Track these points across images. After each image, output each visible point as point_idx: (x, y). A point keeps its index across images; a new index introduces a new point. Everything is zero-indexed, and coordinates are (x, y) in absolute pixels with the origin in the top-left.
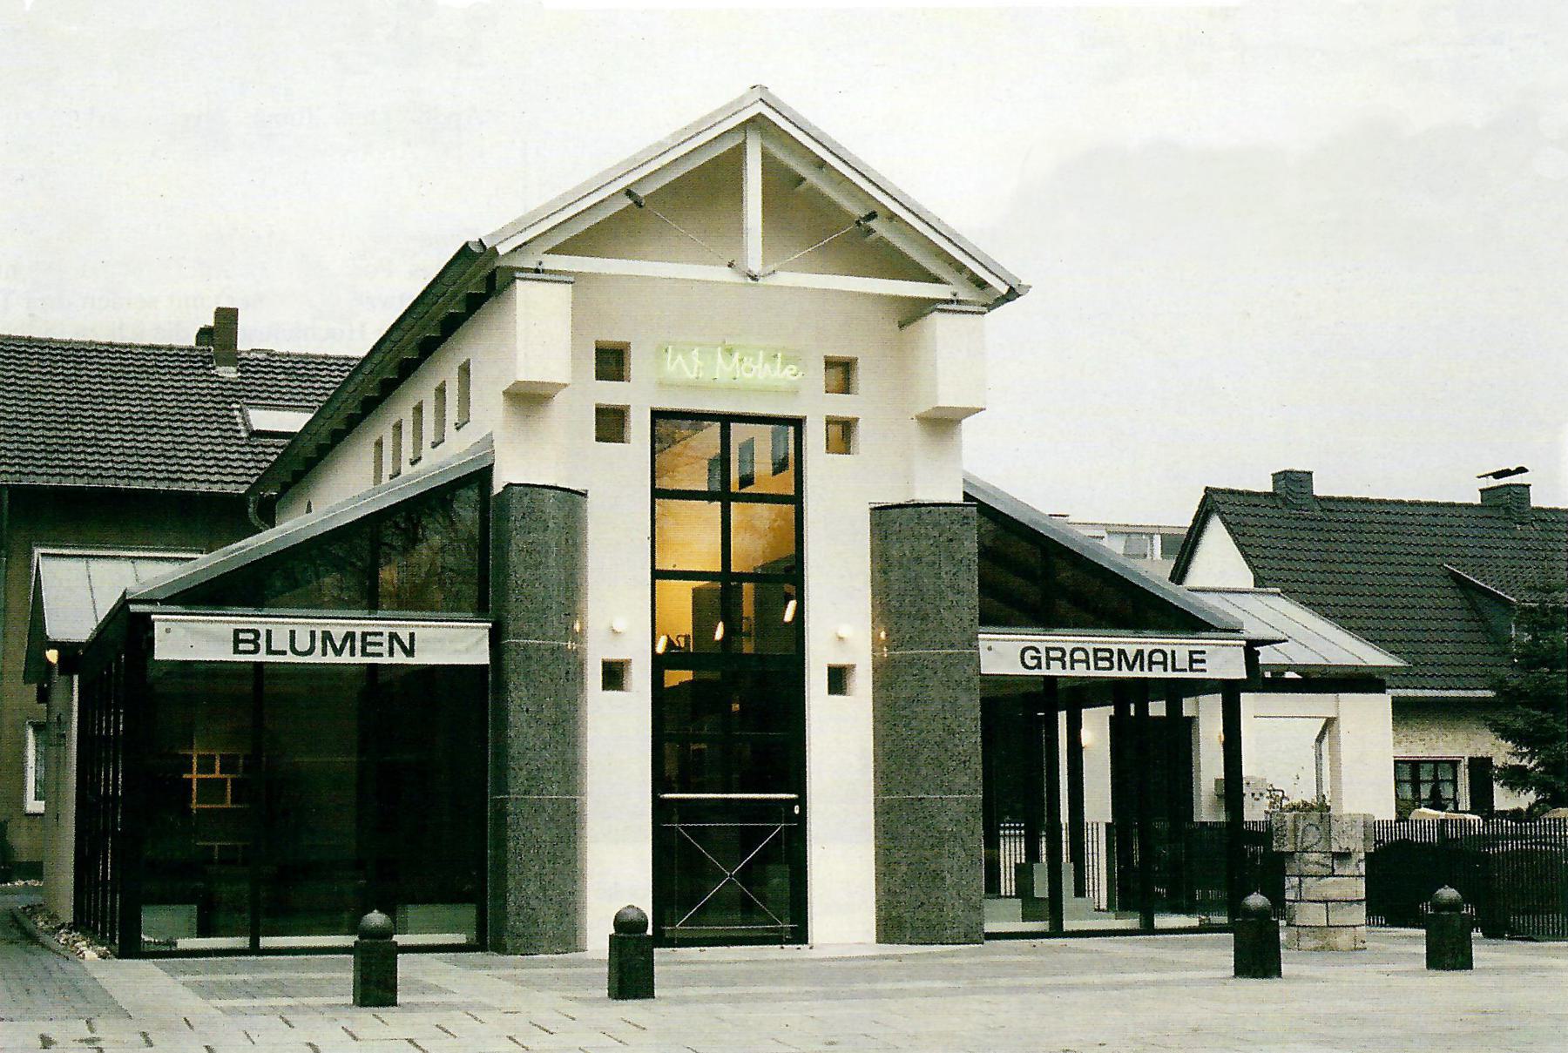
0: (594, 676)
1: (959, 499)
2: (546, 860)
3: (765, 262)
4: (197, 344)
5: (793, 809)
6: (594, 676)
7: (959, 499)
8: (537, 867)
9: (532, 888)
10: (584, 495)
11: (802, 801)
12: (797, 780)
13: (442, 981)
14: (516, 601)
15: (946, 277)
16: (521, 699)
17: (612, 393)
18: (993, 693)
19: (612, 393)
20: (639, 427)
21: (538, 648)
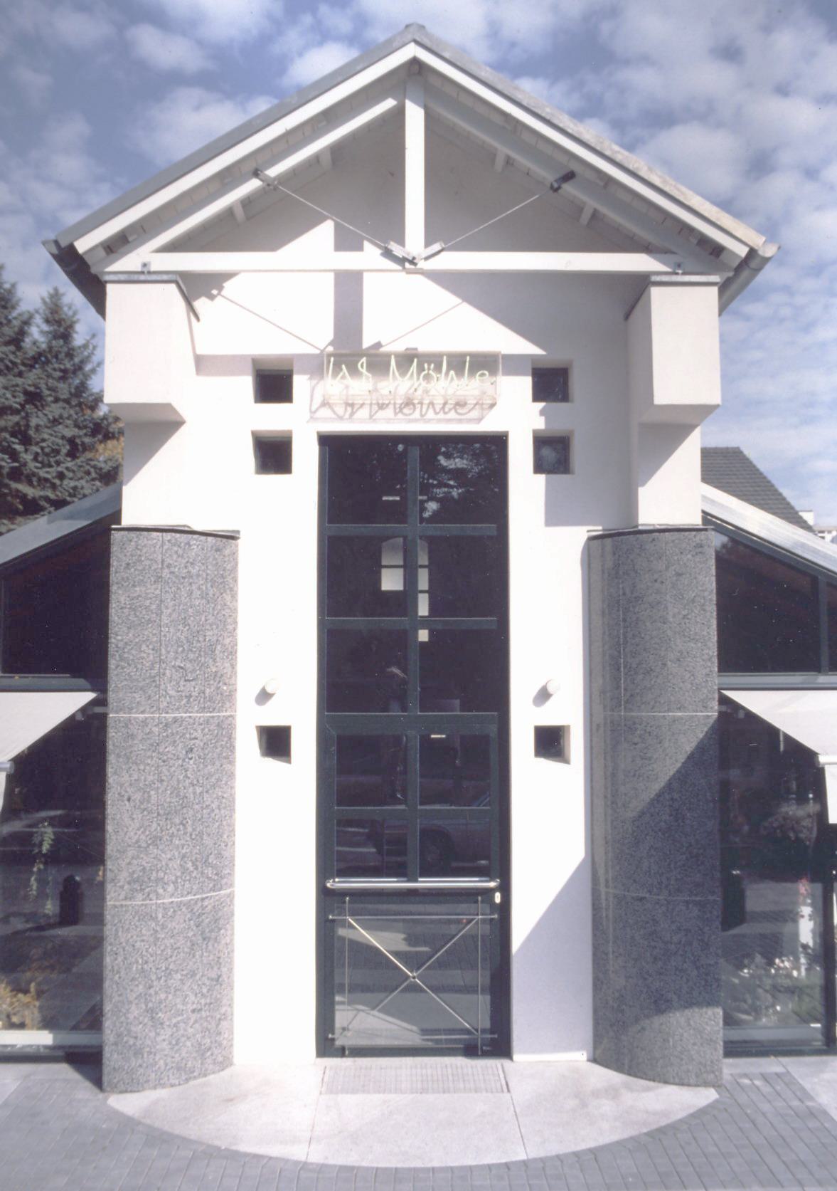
0: (576, 744)
1: (697, 521)
2: (154, 977)
3: (427, 244)
4: (703, 524)
5: (493, 897)
6: (576, 744)
7: (697, 521)
8: (141, 987)
9: (135, 1012)
10: (232, 537)
11: (505, 888)
12: (501, 867)
13: (424, 1043)
14: (117, 667)
15: (674, 249)
16: (122, 785)
17: (273, 417)
18: (287, 759)
19: (273, 417)
20: (306, 458)
21: (145, 723)
